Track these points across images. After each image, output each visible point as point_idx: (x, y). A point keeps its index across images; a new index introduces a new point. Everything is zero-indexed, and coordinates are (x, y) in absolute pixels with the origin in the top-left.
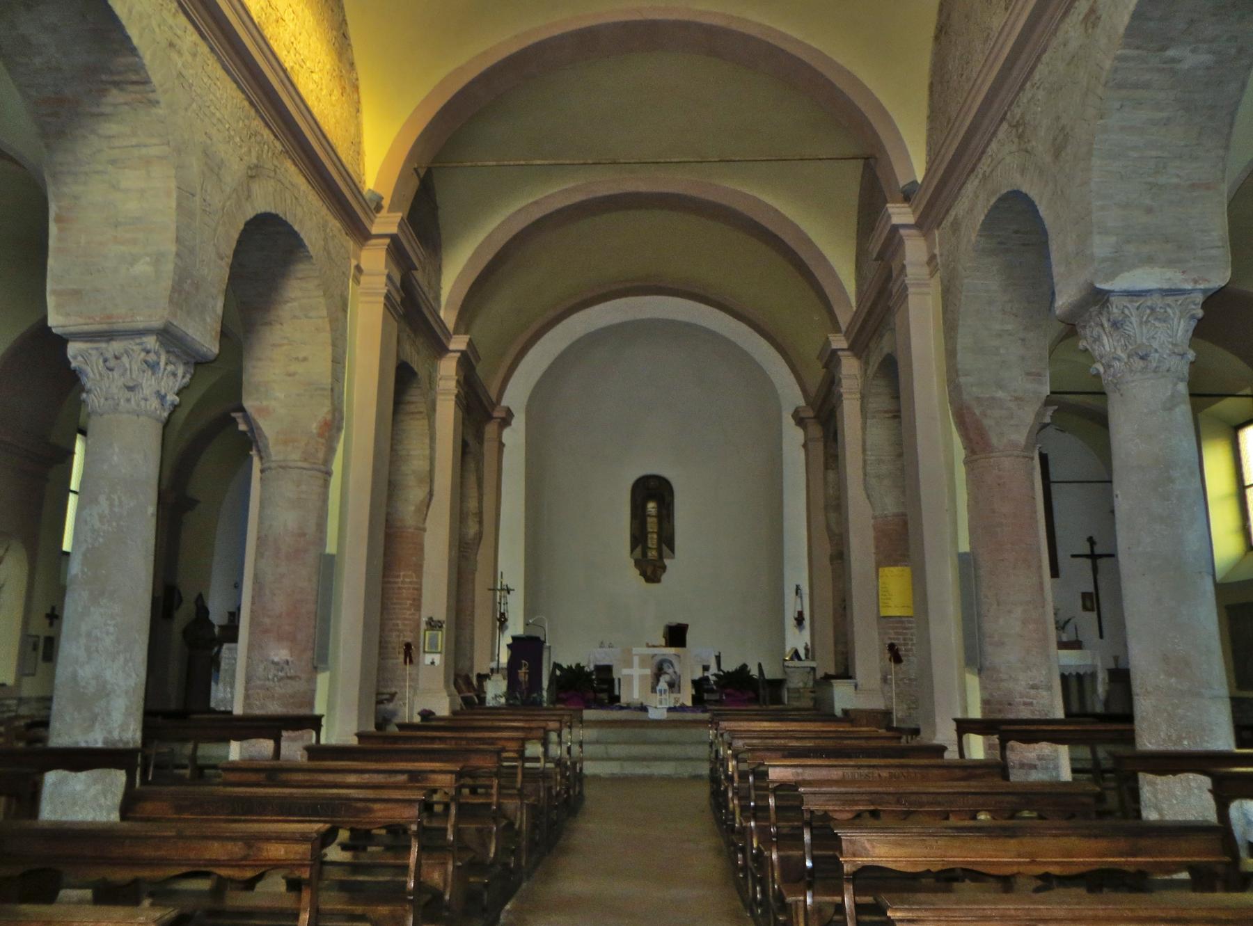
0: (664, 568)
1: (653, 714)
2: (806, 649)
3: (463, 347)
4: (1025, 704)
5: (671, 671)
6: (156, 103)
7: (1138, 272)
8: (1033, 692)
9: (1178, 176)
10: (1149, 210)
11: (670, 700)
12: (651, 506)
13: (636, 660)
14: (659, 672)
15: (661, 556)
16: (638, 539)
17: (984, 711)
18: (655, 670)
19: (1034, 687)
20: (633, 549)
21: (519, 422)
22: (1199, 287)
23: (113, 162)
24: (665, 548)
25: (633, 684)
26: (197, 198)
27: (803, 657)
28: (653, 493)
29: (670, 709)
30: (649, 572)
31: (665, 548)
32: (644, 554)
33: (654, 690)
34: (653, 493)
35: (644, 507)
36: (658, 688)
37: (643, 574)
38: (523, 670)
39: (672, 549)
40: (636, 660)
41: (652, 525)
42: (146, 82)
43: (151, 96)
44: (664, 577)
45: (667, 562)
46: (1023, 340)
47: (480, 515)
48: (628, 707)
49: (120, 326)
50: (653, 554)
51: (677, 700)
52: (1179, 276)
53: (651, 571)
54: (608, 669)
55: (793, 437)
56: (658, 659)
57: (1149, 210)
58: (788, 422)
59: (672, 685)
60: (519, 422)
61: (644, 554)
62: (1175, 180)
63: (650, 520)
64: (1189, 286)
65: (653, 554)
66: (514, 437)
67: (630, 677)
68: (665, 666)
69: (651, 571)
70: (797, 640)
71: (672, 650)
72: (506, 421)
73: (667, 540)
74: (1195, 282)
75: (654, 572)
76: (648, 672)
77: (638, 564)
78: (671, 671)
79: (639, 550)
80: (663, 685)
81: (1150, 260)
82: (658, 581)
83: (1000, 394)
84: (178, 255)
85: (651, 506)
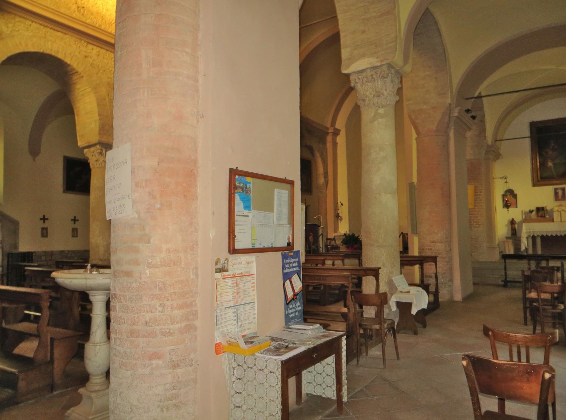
4: (429, 249)
6: (82, 77)
7: (359, 62)
8: (432, 244)
9: (375, 12)
10: (364, 32)
17: (419, 252)
19: (433, 242)
21: (343, 134)
22: (383, 63)
23: (82, 95)
26: (107, 100)
38: (311, 237)
42: (77, 72)
43: (81, 75)
46: (436, 78)
49: (91, 143)
52: (376, 60)
57: (364, 32)
60: (343, 134)
62: (374, 14)
64: (379, 64)
72: (336, 133)
74: (382, 61)
81: (363, 56)
83: (425, 107)
84: (100, 119)
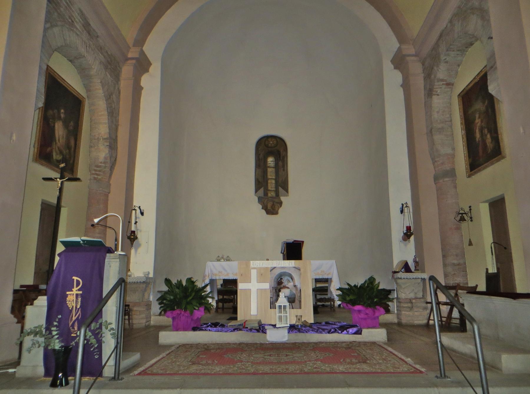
0: (281, 203)
1: (274, 336)
2: (415, 262)
3: (137, 55)
5: (290, 285)
11: (291, 317)
12: (271, 160)
13: (254, 274)
14: (278, 286)
15: (278, 195)
16: (261, 183)
18: (274, 284)
20: (256, 191)
21: (155, 69)
24: (280, 189)
25: (253, 299)
27: (413, 269)
28: (271, 151)
29: (292, 328)
30: (269, 207)
31: (280, 189)
32: (266, 194)
33: (272, 305)
34: (271, 151)
35: (265, 161)
36: (277, 304)
37: (265, 208)
39: (286, 190)
40: (254, 274)
41: (271, 173)
44: (281, 210)
45: (282, 198)
47: (113, 144)
48: (242, 327)
50: (272, 194)
51: (299, 318)
53: (271, 206)
54: (234, 282)
55: (393, 78)
56: (277, 272)
58: (388, 67)
59: (292, 300)
60: (155, 69)
61: (266, 194)
63: (269, 170)
65: (272, 194)
66: (151, 83)
67: (259, 281)
68: (285, 280)
69: (271, 206)
70: (403, 252)
71: (292, 263)
73: (283, 184)
75: (273, 206)
76: (266, 286)
77: (260, 200)
78: (290, 285)
79: (261, 192)
80: (282, 300)
82: (276, 213)
85: (271, 160)
